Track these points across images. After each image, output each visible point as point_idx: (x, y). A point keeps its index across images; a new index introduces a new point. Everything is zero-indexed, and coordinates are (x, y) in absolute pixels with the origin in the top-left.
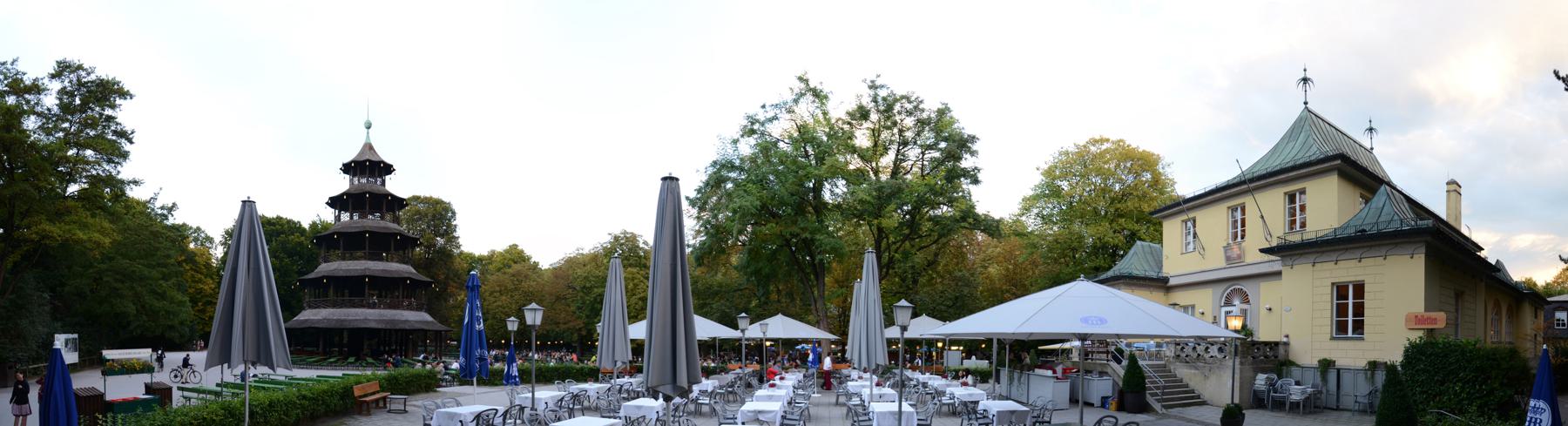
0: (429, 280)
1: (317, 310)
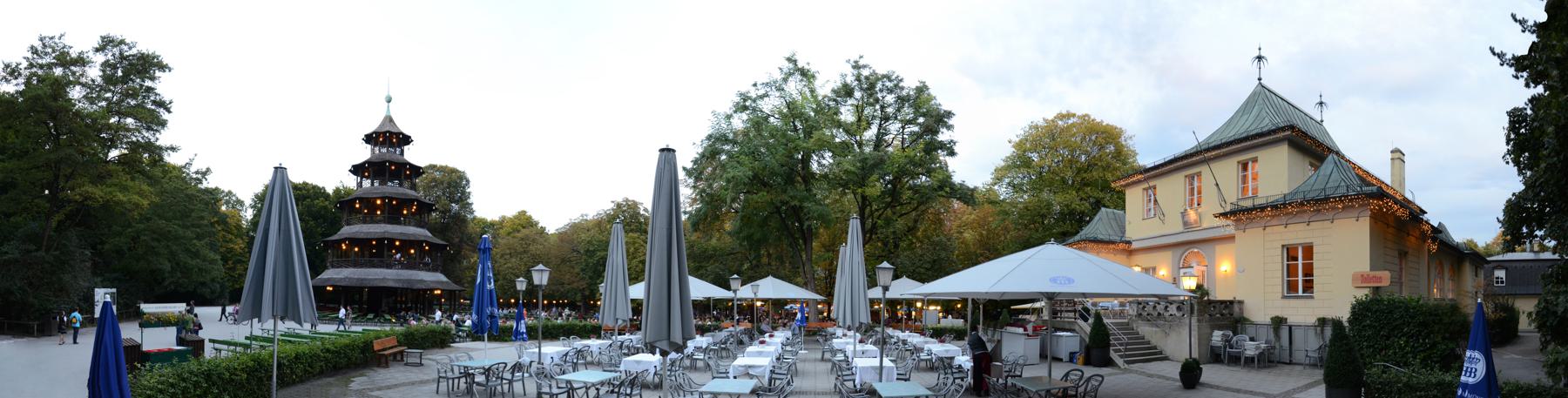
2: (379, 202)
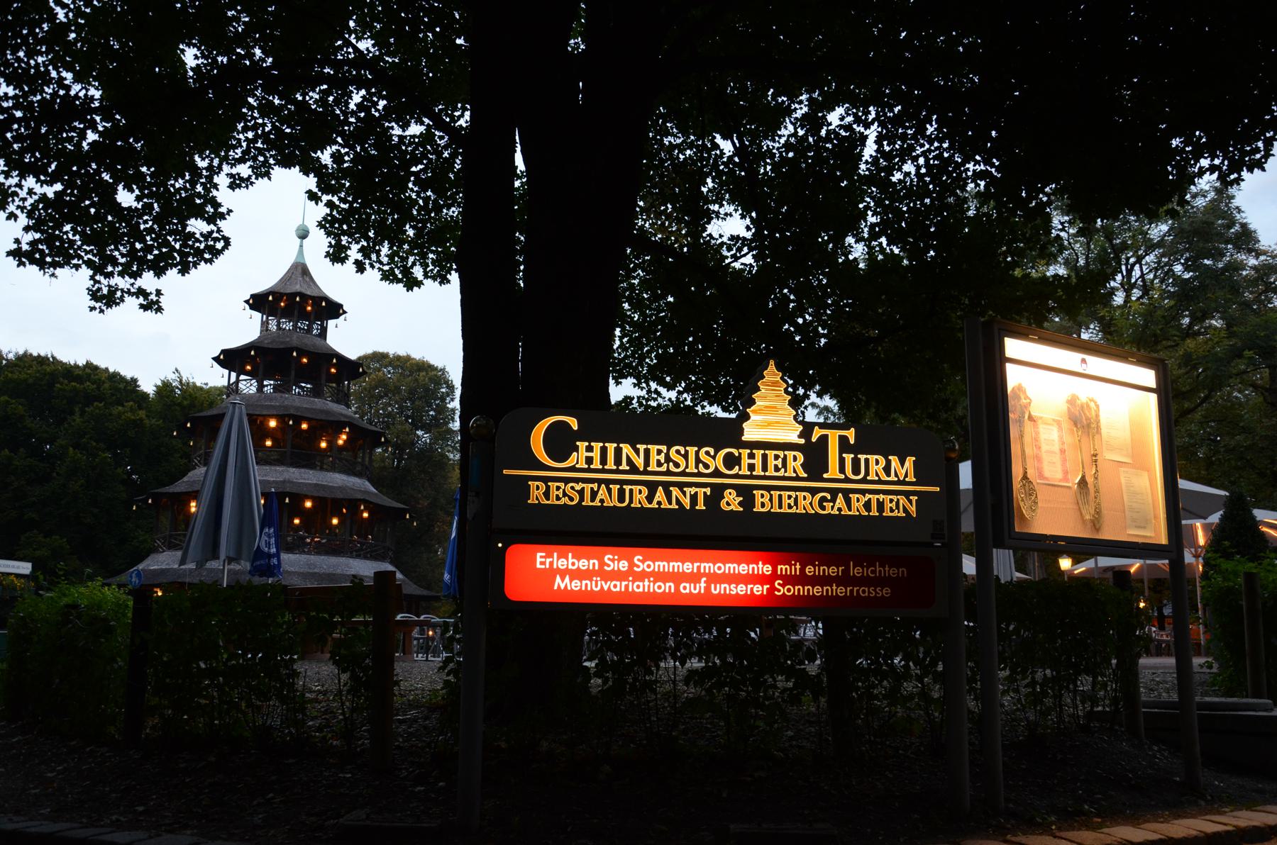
0: (402, 506)
2: (273, 424)
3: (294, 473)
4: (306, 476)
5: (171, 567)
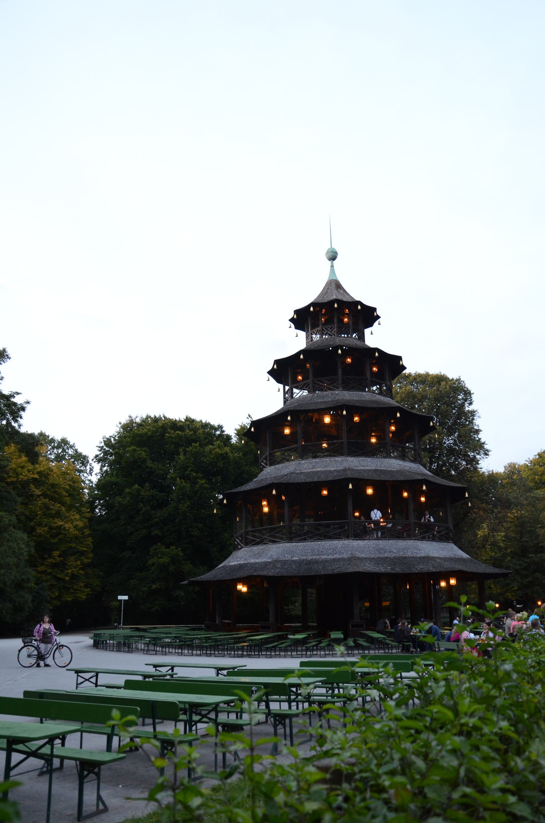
1: (261, 547)
3: (353, 461)
4: (365, 463)
5: (248, 562)
